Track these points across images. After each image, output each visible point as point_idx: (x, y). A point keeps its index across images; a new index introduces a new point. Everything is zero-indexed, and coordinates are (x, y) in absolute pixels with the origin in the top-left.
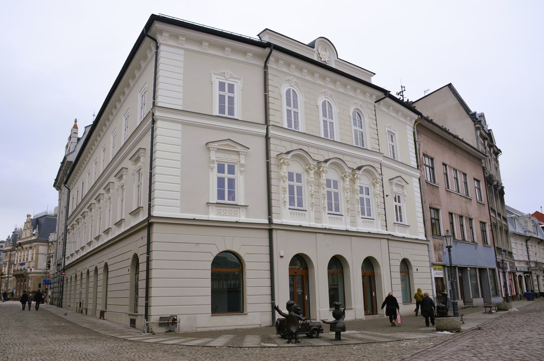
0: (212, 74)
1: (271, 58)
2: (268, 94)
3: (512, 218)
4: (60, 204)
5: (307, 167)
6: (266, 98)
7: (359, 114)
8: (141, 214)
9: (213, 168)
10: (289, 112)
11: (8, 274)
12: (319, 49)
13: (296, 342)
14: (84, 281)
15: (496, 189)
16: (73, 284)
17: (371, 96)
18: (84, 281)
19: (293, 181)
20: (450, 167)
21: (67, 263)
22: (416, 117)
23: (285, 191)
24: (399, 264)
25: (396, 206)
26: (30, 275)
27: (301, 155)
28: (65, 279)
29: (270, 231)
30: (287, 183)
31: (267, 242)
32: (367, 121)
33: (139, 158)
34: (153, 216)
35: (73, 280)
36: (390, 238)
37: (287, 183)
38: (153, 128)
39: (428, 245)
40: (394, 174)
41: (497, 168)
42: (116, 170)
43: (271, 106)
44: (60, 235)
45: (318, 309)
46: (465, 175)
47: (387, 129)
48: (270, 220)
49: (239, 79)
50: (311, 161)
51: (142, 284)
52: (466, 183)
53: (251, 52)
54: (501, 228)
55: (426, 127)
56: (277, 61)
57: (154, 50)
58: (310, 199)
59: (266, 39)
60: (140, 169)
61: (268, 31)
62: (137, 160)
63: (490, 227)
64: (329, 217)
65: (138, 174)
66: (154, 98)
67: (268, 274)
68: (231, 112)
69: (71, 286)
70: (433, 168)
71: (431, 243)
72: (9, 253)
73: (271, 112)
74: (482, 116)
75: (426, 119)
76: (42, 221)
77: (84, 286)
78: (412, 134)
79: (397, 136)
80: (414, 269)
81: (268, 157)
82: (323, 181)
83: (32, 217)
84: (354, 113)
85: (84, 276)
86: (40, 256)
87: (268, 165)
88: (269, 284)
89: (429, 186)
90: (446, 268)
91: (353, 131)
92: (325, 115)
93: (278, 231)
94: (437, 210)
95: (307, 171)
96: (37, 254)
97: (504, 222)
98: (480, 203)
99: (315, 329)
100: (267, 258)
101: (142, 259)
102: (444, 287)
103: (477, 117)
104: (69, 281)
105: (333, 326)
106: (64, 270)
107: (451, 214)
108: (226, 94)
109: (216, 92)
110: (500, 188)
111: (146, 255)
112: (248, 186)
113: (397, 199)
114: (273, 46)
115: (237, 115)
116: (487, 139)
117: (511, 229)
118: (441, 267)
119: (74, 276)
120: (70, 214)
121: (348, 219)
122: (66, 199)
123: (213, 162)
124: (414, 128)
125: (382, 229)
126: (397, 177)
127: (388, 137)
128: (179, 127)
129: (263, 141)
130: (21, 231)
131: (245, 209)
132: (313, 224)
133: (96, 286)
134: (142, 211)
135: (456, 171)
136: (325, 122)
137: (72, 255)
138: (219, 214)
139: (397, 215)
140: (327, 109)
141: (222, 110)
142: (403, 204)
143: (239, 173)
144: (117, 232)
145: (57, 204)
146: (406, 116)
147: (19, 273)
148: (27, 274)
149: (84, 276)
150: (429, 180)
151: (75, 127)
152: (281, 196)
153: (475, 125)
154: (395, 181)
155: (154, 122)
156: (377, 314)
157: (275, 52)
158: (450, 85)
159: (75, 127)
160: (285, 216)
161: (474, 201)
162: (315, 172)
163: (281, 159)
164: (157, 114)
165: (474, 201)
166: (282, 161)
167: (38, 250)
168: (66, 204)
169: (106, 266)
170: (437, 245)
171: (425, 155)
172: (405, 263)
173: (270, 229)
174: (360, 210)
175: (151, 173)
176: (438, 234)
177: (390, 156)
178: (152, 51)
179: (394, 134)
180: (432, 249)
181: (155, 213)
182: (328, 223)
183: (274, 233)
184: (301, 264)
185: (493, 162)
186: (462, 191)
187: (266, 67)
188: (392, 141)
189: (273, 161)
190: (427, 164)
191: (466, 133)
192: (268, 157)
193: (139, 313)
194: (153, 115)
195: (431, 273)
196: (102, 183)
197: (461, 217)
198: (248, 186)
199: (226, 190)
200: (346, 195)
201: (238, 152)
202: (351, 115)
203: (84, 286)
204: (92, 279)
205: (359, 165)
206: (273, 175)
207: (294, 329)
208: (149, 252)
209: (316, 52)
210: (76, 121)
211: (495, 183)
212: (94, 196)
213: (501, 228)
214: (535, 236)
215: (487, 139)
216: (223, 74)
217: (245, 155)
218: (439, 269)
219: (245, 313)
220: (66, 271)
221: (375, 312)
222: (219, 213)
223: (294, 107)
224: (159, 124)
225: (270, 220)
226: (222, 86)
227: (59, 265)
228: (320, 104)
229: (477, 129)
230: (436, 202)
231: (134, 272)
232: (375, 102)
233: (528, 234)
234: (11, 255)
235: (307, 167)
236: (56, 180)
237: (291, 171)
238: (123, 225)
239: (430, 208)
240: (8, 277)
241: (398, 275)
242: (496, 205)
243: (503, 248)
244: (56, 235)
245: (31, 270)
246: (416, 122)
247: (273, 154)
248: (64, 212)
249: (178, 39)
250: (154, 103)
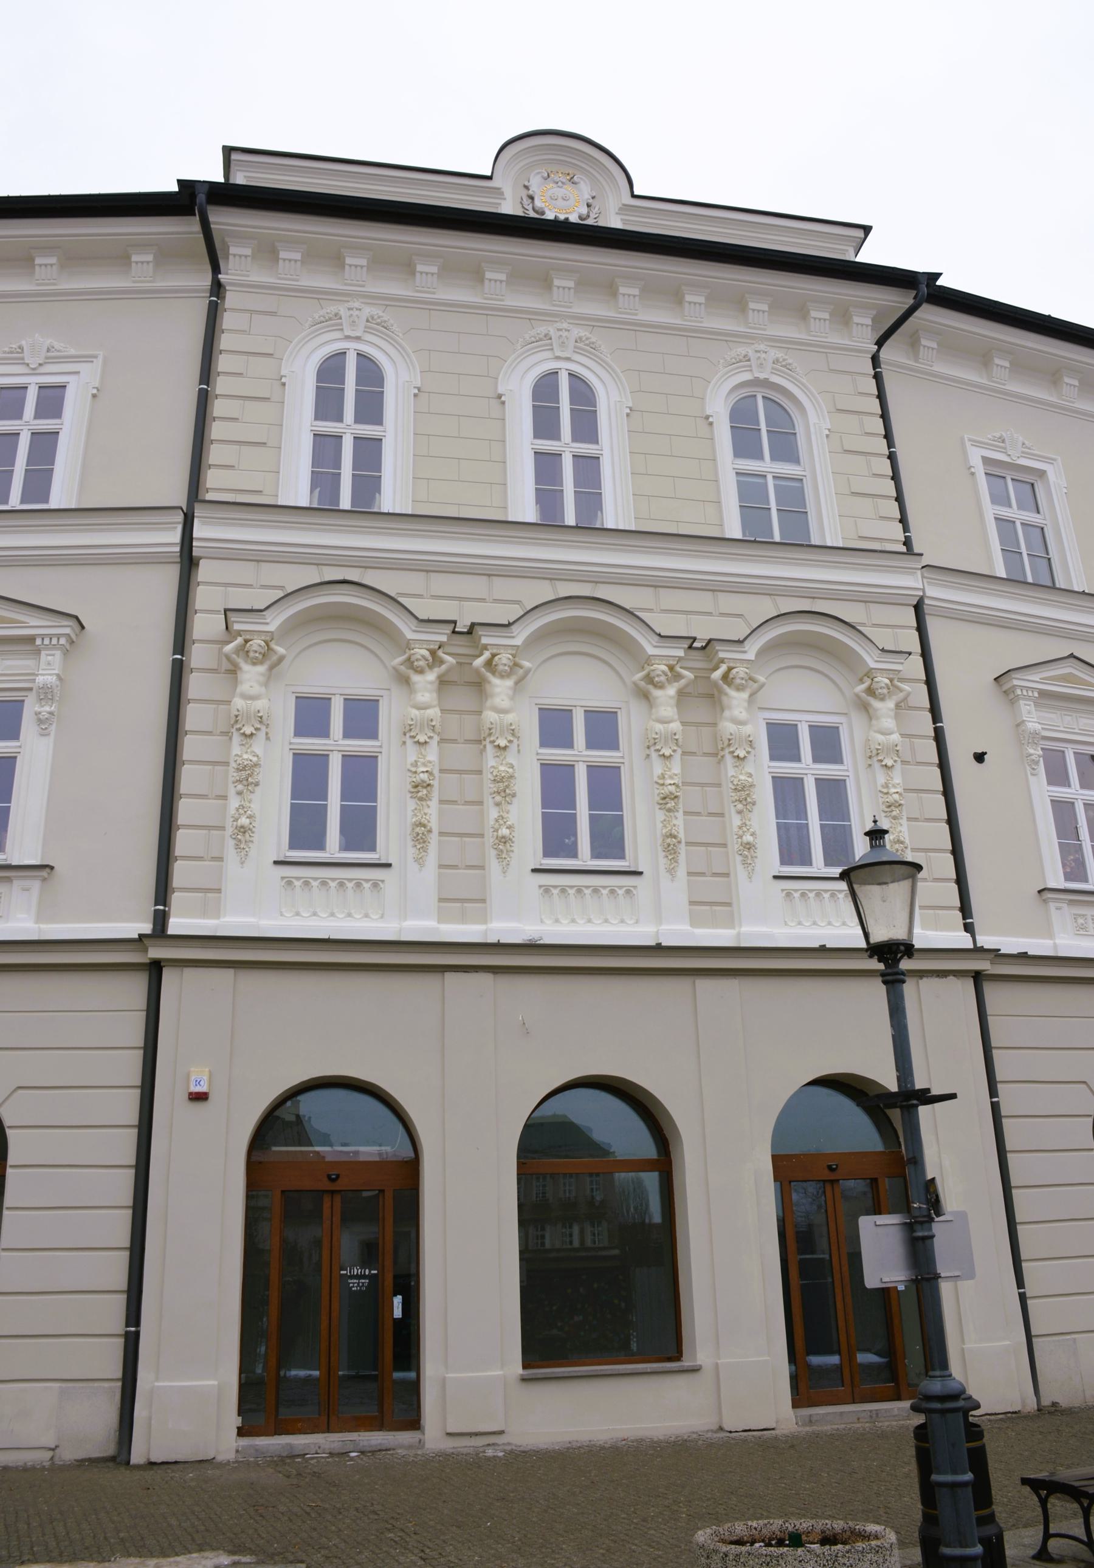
0: (968, 444)
6: (204, 400)
48: (161, 920)
49: (89, 359)
53: (142, 246)
56: (268, 253)
64: (546, 890)
87: (178, 673)
88: (125, 1240)
93: (189, 973)
95: (865, 708)
131: (36, 885)
132: (423, 925)
162: (443, 682)
179: (1042, 474)
200: (658, 770)
201: (31, 639)
219: (686, 1363)
222: (1083, 927)
228: (719, 408)
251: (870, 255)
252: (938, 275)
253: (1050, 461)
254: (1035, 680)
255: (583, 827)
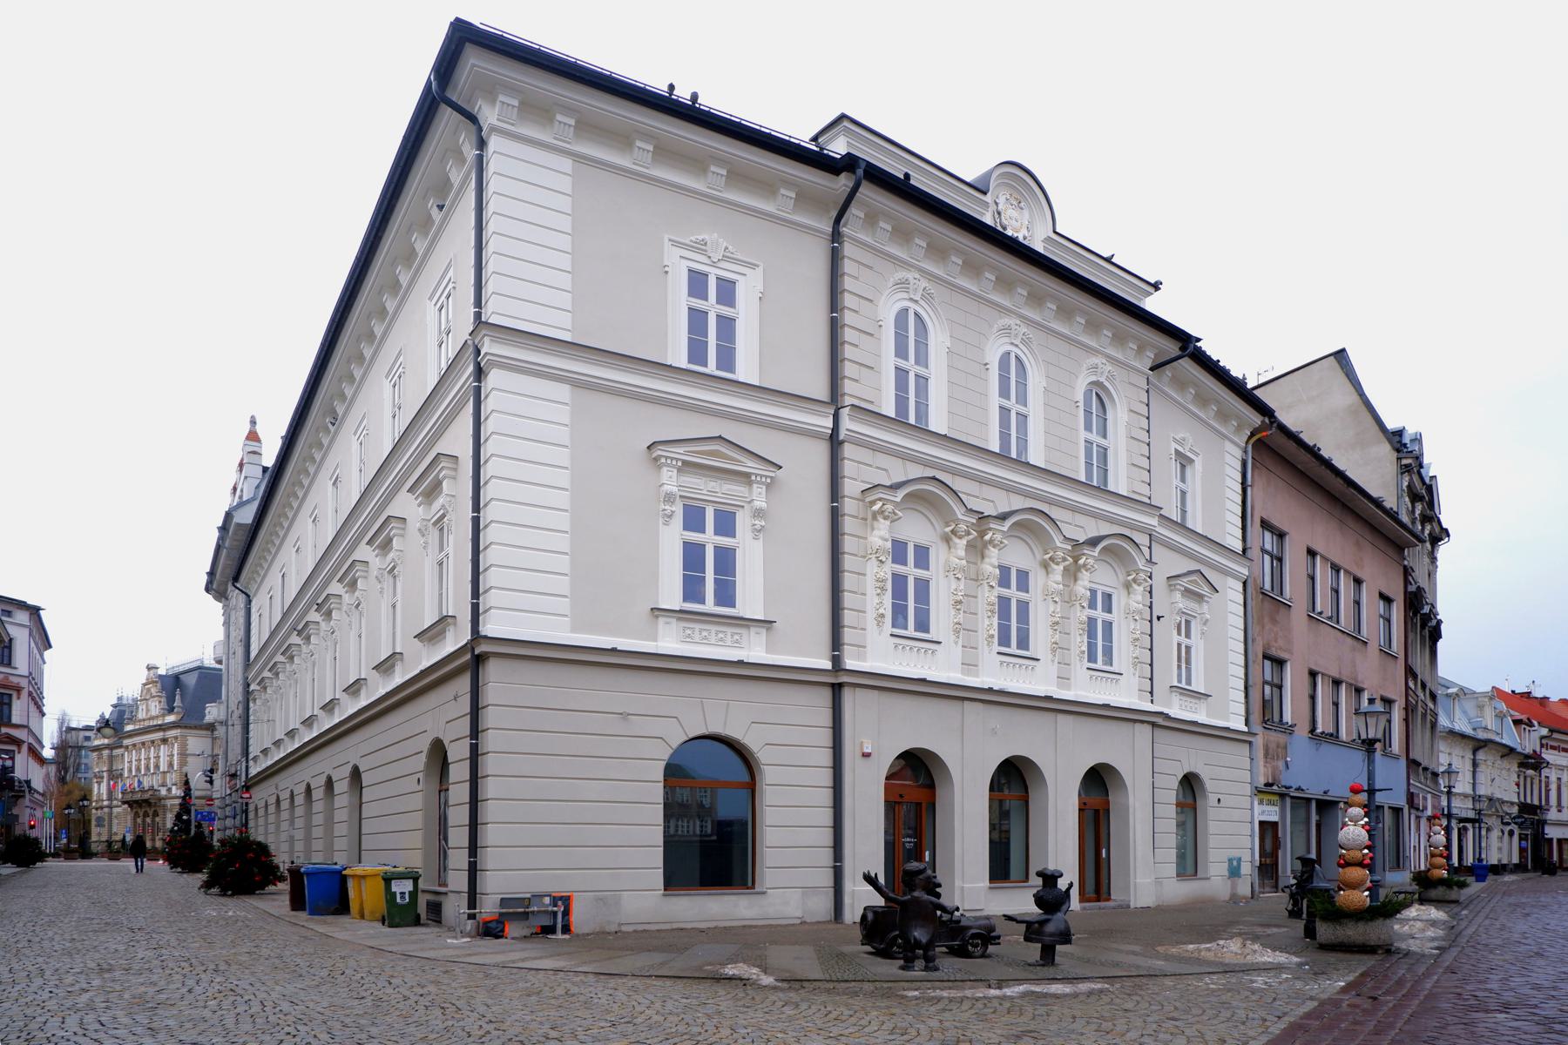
1: (854, 211)
2: (842, 316)
3: (1448, 695)
4: (228, 636)
5: (948, 529)
6: (835, 327)
7: (1099, 397)
8: (450, 635)
9: (670, 516)
10: (901, 374)
11: (110, 798)
12: (1001, 200)
13: (926, 969)
14: (299, 811)
15: (1423, 626)
16: (272, 819)
17: (1141, 349)
18: (299, 811)
19: (905, 563)
20: (1323, 557)
21: (253, 771)
22: (1257, 419)
23: (883, 589)
24: (1175, 785)
25: (1179, 645)
26: (169, 803)
27: (927, 496)
28: (251, 807)
29: (837, 689)
30: (889, 568)
31: (826, 717)
32: (1119, 416)
33: (437, 485)
34: (486, 637)
35: (272, 809)
36: (1160, 723)
37: (889, 568)
38: (478, 391)
39: (1250, 743)
40: (1186, 565)
41: (1431, 575)
42: (371, 525)
43: (848, 352)
44: (233, 706)
45: (958, 883)
46: (1358, 581)
47: (1174, 446)
48: (836, 661)
49: (753, 266)
50: (959, 512)
51: (458, 816)
52: (1357, 603)
54: (1424, 715)
55: (1279, 452)
57: (470, 153)
58: (953, 612)
59: (838, 147)
60: (443, 516)
61: (846, 123)
62: (434, 490)
63: (1403, 713)
65: (437, 533)
66: (478, 303)
67: (826, 797)
68: (727, 358)
69: (267, 824)
70: (1280, 560)
71: (1259, 741)
72: (106, 752)
73: (849, 369)
74: (1418, 439)
75: (1283, 429)
76: (191, 681)
77: (299, 823)
78: (1238, 466)
79: (1198, 462)
80: (1212, 799)
81: (835, 492)
82: (990, 567)
83: (162, 672)
84: (1088, 393)
85: (300, 800)
86: (190, 759)
87: (835, 516)
89: (1265, 603)
90: (1288, 800)
91: (1082, 444)
92: (1004, 392)
94: (1279, 663)
96: (184, 755)
97: (1431, 705)
98: (1386, 654)
99: (975, 936)
100: (826, 757)
101: (458, 752)
102: (1277, 844)
103: (1406, 440)
104: (261, 812)
105: (1033, 930)
106: (247, 788)
107: (1313, 674)
108: (712, 307)
109: (680, 301)
110: (1434, 622)
111: (467, 741)
112: (773, 572)
113: (1185, 628)
114: (863, 165)
115: (746, 369)
116: (1421, 499)
117: (1443, 721)
118: (1276, 798)
119: (273, 800)
120: (253, 655)
121: (1053, 670)
122: (242, 620)
123: (669, 498)
124: (1245, 452)
125: (1140, 698)
126: (1190, 573)
127: (1174, 467)
128: (563, 391)
129: (821, 451)
130: (134, 705)
133: (329, 822)
134: (451, 628)
135: (1338, 571)
136: (1004, 411)
137: (265, 752)
138: (688, 639)
139: (1179, 667)
140: (1012, 375)
141: (697, 351)
142: (1196, 642)
143: (749, 535)
144: (381, 687)
145: (220, 634)
146: (1223, 416)
147: (138, 797)
148: (160, 799)
149: (300, 800)
150: (1268, 586)
151: (253, 436)
152: (869, 596)
153: (1399, 459)
154: (1184, 582)
155: (479, 373)
156: (1108, 899)
157: (868, 192)
158: (1340, 356)
159: (253, 436)
160: (877, 651)
161: (1373, 648)
163: (873, 503)
164: (487, 347)
165: (1373, 648)
166: (876, 507)
167: (183, 747)
168: (242, 632)
169: (356, 774)
170: (1272, 746)
171: (1265, 525)
172: (1190, 782)
173: (837, 685)
174: (1085, 648)
175: (476, 522)
176: (1276, 719)
177: (1175, 516)
178: (464, 161)
179: (1191, 461)
180: (1260, 754)
181: (490, 628)
182: (994, 674)
183: (847, 695)
184: (917, 776)
185: (1427, 560)
186: (1345, 621)
187: (836, 236)
188: (1183, 480)
189: (849, 506)
190: (1268, 547)
191: (1374, 474)
192: (835, 492)
193: (451, 887)
194: (478, 352)
195: (1252, 809)
196: (337, 565)
197: (1337, 683)
198: (773, 572)
199: (708, 577)
201: (748, 475)
202: (1080, 397)
203: (299, 823)
204: (318, 806)
205: (1093, 533)
206: (848, 544)
207: (920, 934)
208: (475, 732)
209: (993, 207)
210: (253, 422)
211: (1426, 609)
212: (314, 600)
213: (1424, 715)
214: (1498, 739)
215: (1421, 499)
216: (700, 247)
217: (768, 486)
218: (1270, 803)
220: (253, 791)
221: (1104, 896)
223: (917, 362)
224: (494, 378)
225: (836, 661)
226: (697, 283)
227: (233, 776)
229: (1406, 469)
230: (1281, 643)
231: (436, 786)
232: (1152, 369)
233: (1481, 735)
234: (111, 758)
235: (948, 529)
236: (211, 574)
237: (901, 537)
238: (398, 668)
239: (1266, 657)
240: (110, 807)
241: (1171, 811)
242: (1419, 663)
243: (1425, 763)
244: (223, 707)
245: (169, 790)
246: (1252, 434)
247: (850, 487)
248: (240, 651)
249: (551, 120)
250: (478, 316)
251: (1152, 304)
252: (1199, 340)
253: (1197, 454)
254: (679, 452)
255: (1013, 633)
